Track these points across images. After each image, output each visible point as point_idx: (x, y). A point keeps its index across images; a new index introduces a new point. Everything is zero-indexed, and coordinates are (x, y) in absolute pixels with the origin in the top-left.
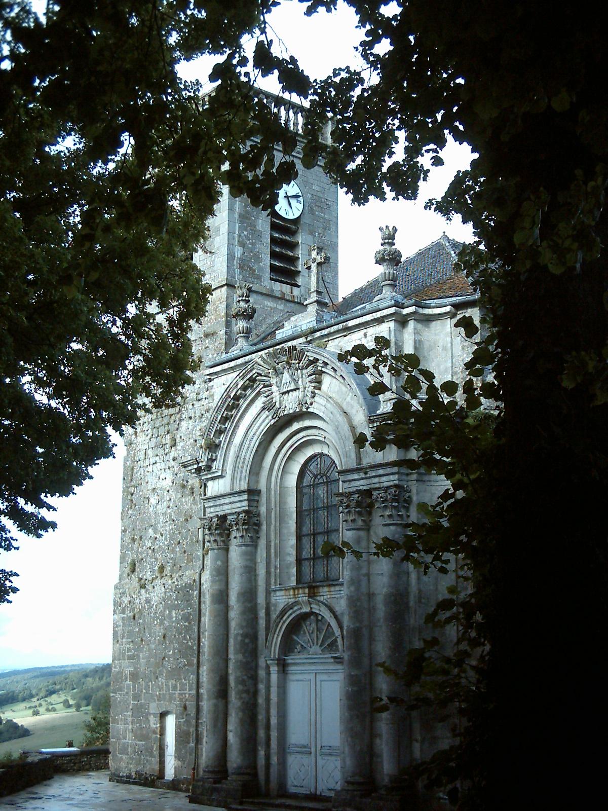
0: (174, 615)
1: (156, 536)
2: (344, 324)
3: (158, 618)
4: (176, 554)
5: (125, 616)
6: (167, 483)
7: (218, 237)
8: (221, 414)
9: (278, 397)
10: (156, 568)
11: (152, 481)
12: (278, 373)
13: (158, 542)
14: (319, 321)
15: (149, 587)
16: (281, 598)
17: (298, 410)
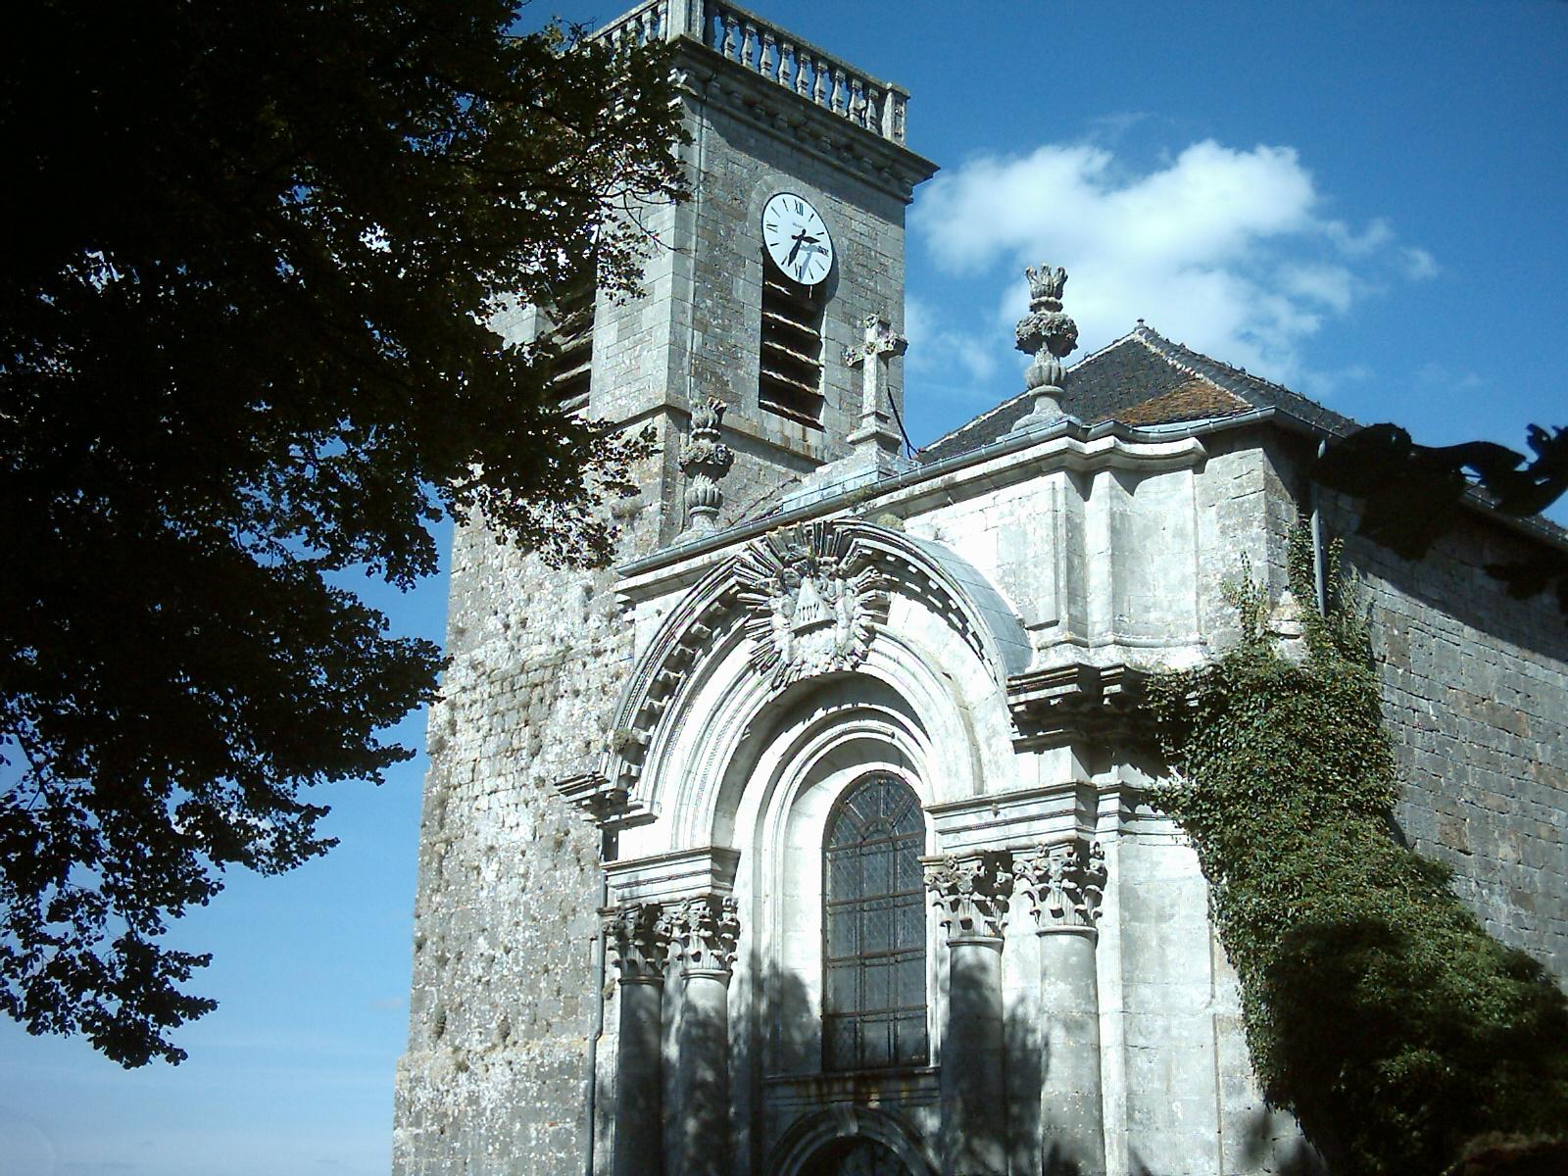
0: (534, 1134)
1: (493, 953)
2: (946, 476)
3: (496, 1138)
4: (539, 995)
5: (421, 1131)
6: (524, 834)
7: (650, 308)
8: (654, 674)
9: (787, 639)
10: (494, 1025)
11: (488, 832)
12: (786, 587)
13: (497, 967)
14: (884, 473)
15: (478, 1068)
16: (789, 1101)
17: (832, 669)
